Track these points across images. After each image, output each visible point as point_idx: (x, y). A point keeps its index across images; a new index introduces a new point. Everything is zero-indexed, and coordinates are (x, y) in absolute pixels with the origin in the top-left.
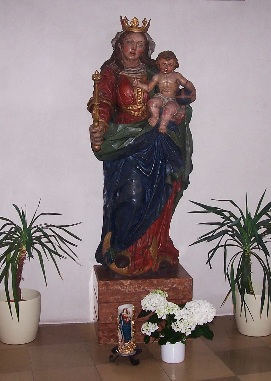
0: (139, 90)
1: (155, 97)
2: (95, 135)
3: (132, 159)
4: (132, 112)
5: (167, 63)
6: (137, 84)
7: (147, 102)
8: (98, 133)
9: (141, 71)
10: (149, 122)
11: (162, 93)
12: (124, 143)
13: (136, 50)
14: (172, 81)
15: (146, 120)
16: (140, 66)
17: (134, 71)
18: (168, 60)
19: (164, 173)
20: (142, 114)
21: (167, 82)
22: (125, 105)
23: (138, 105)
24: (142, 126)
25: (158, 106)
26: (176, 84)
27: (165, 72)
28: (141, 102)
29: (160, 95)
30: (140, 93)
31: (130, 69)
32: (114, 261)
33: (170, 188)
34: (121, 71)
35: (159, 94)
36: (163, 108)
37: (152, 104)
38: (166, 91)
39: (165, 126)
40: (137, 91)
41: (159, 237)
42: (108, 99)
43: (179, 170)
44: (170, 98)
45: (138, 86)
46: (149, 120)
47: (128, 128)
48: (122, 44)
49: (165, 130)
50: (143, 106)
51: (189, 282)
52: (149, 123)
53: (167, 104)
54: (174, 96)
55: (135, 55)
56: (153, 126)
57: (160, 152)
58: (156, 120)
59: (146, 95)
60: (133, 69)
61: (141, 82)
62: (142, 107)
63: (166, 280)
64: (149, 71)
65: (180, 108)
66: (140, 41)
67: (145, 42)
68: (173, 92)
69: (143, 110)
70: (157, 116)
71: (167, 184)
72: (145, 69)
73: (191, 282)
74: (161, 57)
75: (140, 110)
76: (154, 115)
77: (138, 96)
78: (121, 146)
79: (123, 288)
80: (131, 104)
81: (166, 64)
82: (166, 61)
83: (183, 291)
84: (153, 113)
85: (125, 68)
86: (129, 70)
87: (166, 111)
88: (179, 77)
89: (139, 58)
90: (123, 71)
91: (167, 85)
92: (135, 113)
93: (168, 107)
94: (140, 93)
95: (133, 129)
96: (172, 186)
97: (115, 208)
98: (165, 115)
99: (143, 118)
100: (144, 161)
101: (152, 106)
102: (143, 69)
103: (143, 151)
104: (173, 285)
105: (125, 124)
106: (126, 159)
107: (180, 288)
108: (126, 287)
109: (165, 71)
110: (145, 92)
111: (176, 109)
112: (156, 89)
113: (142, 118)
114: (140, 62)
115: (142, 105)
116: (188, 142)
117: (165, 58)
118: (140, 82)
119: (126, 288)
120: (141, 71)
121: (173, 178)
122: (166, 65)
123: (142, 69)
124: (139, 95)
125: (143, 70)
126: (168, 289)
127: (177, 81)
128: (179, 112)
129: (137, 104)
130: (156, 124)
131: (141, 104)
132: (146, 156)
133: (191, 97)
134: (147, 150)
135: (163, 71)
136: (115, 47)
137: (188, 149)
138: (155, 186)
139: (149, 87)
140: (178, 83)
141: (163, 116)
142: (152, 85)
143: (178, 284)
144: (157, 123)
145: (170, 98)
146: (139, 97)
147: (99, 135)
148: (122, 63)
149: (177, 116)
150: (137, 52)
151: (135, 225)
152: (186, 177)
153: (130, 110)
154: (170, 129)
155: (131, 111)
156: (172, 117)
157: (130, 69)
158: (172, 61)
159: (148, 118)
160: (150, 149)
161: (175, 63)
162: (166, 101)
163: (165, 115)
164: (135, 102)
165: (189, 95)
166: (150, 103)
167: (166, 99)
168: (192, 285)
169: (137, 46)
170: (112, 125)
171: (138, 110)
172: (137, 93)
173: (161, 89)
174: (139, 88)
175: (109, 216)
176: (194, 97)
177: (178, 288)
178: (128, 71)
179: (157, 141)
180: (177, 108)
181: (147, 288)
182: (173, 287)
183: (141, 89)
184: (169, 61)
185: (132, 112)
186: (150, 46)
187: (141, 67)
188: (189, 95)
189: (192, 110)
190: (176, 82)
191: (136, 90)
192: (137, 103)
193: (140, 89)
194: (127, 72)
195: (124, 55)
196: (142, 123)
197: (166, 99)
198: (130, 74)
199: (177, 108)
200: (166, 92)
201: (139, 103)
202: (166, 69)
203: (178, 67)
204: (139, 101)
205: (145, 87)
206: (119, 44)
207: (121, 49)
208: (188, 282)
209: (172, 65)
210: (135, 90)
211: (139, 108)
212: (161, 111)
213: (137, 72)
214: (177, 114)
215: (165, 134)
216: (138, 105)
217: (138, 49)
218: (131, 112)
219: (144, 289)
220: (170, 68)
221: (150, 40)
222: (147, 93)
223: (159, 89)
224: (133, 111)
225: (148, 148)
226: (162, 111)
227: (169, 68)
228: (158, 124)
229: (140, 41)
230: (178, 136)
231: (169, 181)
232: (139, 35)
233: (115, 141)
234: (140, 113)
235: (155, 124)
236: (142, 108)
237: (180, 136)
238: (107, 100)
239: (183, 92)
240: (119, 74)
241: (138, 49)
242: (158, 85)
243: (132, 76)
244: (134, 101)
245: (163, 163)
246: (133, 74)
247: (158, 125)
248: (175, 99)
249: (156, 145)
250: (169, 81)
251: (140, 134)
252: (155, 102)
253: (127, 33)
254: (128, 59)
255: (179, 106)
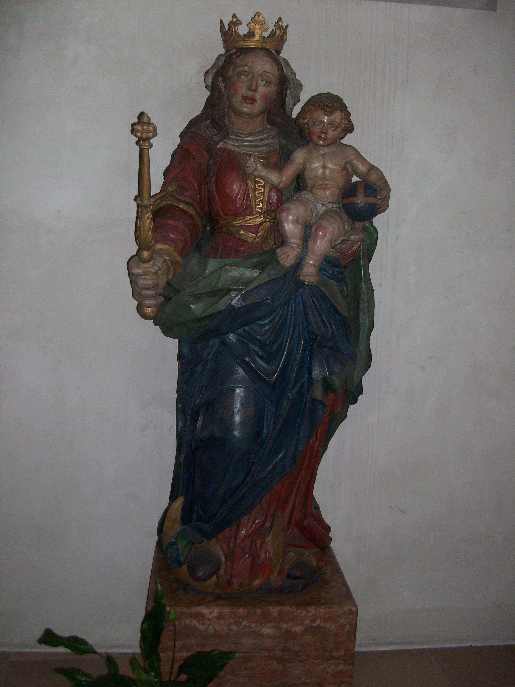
0: (260, 183)
1: (295, 200)
2: (143, 282)
3: (235, 340)
4: (242, 232)
5: (326, 119)
6: (255, 169)
7: (275, 211)
8: (148, 277)
9: (266, 142)
10: (278, 255)
11: (311, 192)
12: (216, 302)
13: (255, 91)
14: (335, 165)
15: (273, 252)
16: (267, 131)
17: (251, 141)
18: (328, 112)
19: (306, 376)
20: (265, 239)
21: (324, 167)
22: (226, 215)
23: (255, 216)
24: (262, 266)
25: (300, 221)
26: (344, 172)
27: (321, 142)
28: (264, 211)
29: (307, 196)
30: (261, 190)
31: (243, 136)
32: (186, 562)
33: (320, 406)
34: (222, 139)
35: (304, 193)
36: (311, 226)
37: (288, 216)
38: (321, 187)
39: (314, 266)
40: (255, 186)
41: (289, 507)
42: (188, 200)
43: (343, 369)
44: (329, 203)
45: (257, 173)
46: (278, 251)
47: (226, 268)
48: (225, 78)
49: (314, 276)
50: (268, 220)
51: (351, 616)
52: (279, 259)
53: (321, 217)
54: (339, 199)
55: (253, 103)
56: (287, 265)
57: (299, 327)
58: (296, 253)
59: (275, 197)
60: (249, 136)
61: (266, 166)
62: (265, 222)
63: (298, 611)
64: (284, 142)
65: (352, 228)
66: (267, 71)
67: (279, 77)
68: (337, 191)
69: (266, 228)
70: (296, 244)
71: (314, 400)
72: (277, 137)
73: (355, 616)
74: (313, 105)
75: (261, 228)
76: (289, 241)
77: (256, 197)
78: (211, 309)
79: (203, 624)
80: (240, 215)
81: (323, 122)
82: (323, 115)
83: (336, 635)
84: (289, 235)
85: (232, 135)
86: (241, 139)
87: (320, 231)
88: (351, 156)
89: (262, 112)
90: (226, 140)
91: (324, 173)
92: (249, 235)
93: (324, 223)
94: (261, 190)
95: (236, 272)
96: (324, 405)
97: (193, 447)
98: (317, 242)
99: (265, 248)
100: (262, 345)
101: (287, 220)
102: (272, 138)
103: (261, 323)
104: (315, 621)
105: (225, 258)
106: (221, 338)
107: (328, 628)
108: (208, 622)
109: (320, 138)
110: (274, 187)
111: (342, 228)
112: (298, 183)
113: (263, 246)
114: (266, 123)
115: (264, 217)
116: (363, 305)
117: (322, 109)
118: (263, 165)
119: (210, 624)
120: (266, 142)
121: (327, 386)
122: (322, 125)
123: (269, 138)
124: (258, 193)
125: (271, 141)
126: (303, 628)
127: (347, 166)
128: (349, 238)
129: (253, 215)
130: (295, 262)
131: (262, 216)
132: (268, 335)
133: (380, 202)
134: (271, 322)
135: (315, 138)
136: (213, 88)
137: (363, 320)
138: (286, 405)
139: (283, 178)
140: (350, 169)
141: (310, 243)
142: (290, 171)
143: (326, 620)
144: (296, 260)
145: (330, 204)
146: (258, 199)
147: (150, 282)
148: (227, 123)
149: (343, 246)
150: (258, 96)
151: (237, 487)
152: (356, 380)
153: (236, 226)
154: (327, 276)
155: (240, 231)
156: (333, 248)
157: (243, 136)
158: (337, 116)
159: (277, 248)
160: (277, 319)
161: (344, 121)
162: (321, 209)
163: (315, 241)
164: (248, 210)
165: (375, 197)
166: (282, 211)
167: (320, 205)
168: (355, 622)
169: (260, 82)
170: (195, 261)
171: (255, 229)
172: (255, 190)
173: (310, 183)
174: (261, 178)
175: (182, 459)
176: (385, 202)
177: (325, 628)
178: (237, 141)
179: (295, 302)
180: (344, 226)
181: (257, 626)
182: (314, 625)
183: (264, 180)
184: (330, 115)
185: (242, 232)
186: (290, 88)
187: (268, 133)
188: (375, 197)
189: (378, 235)
190: (345, 168)
191: (251, 182)
192: (255, 213)
193: (261, 181)
194: (236, 144)
195: (231, 106)
196: (263, 257)
197: (319, 205)
198: (241, 148)
199: (344, 226)
200: (321, 188)
201: (258, 213)
202: (323, 133)
203: (351, 132)
204: (258, 208)
205: (274, 177)
206: (220, 79)
207: (225, 90)
208: (348, 615)
209: (337, 125)
210: (249, 183)
211: (257, 223)
212: (308, 232)
213: (258, 143)
214: (343, 240)
215: (315, 285)
216: (256, 217)
217: (262, 90)
218: (238, 231)
219: (249, 627)
220: (333, 132)
221: (290, 75)
222: (279, 190)
223: (304, 182)
224: (243, 229)
225: (273, 315)
226: (310, 233)
227: (331, 134)
228: (299, 263)
229: (267, 72)
230: (342, 292)
231: (318, 392)
232: (265, 58)
233: (198, 297)
234: (259, 236)
235: (292, 262)
236: (264, 224)
237: (347, 290)
238: (186, 203)
239: (360, 192)
240: (218, 146)
241: (262, 90)
242: (303, 172)
243: (246, 152)
244: (246, 208)
245: (307, 353)
246: (249, 148)
247: (298, 265)
248: (341, 205)
249: (292, 309)
250: (330, 166)
251: (256, 284)
252: (293, 211)
253: (239, 53)
254: (238, 114)
255: (348, 221)
